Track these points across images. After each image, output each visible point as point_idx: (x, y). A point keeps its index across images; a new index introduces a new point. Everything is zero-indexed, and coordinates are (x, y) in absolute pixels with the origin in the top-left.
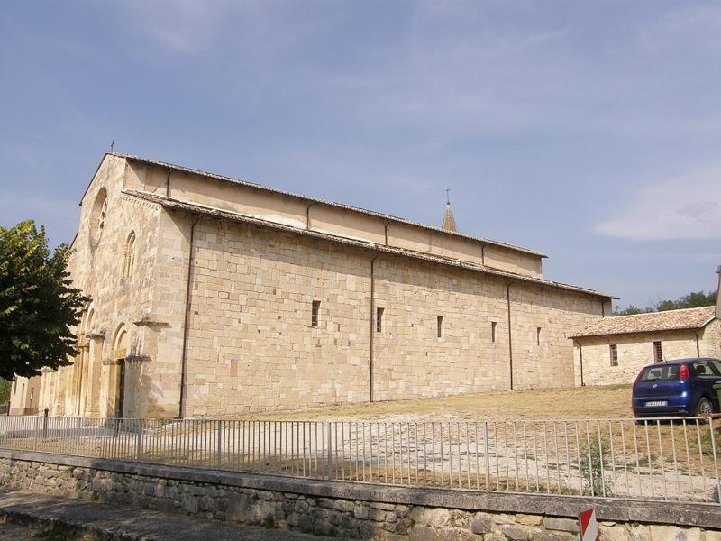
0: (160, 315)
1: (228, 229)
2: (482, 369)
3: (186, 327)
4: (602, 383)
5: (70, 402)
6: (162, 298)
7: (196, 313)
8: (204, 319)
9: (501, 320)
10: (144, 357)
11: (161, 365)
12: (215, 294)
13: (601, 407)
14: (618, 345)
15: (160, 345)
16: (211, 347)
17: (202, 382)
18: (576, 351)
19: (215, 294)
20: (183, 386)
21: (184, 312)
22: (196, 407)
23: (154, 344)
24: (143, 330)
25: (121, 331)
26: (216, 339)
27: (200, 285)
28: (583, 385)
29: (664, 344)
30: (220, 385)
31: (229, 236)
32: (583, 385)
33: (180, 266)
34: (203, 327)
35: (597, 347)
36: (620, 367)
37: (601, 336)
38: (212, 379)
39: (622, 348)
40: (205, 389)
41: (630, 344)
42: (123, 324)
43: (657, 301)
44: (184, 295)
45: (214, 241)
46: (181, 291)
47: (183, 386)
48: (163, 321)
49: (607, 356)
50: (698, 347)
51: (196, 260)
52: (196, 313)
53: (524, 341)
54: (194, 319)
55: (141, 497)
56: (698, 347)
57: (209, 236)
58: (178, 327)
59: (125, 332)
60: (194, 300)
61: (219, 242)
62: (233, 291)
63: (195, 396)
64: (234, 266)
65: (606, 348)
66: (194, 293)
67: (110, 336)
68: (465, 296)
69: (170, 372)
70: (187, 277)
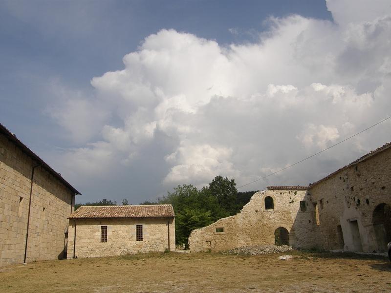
2: (8, 242)
4: (92, 256)
7: (289, 192)
9: (26, 196)
14: (108, 226)
18: (71, 230)
28: (75, 257)
29: (145, 227)
32: (75, 257)
35: (91, 226)
36: (109, 243)
37: (96, 219)
39: (111, 229)
41: (118, 226)
43: (100, 200)
49: (99, 234)
50: (169, 230)
52: (289, 192)
53: (38, 219)
55: (310, 228)
56: (169, 230)
65: (98, 228)
68: (7, 168)
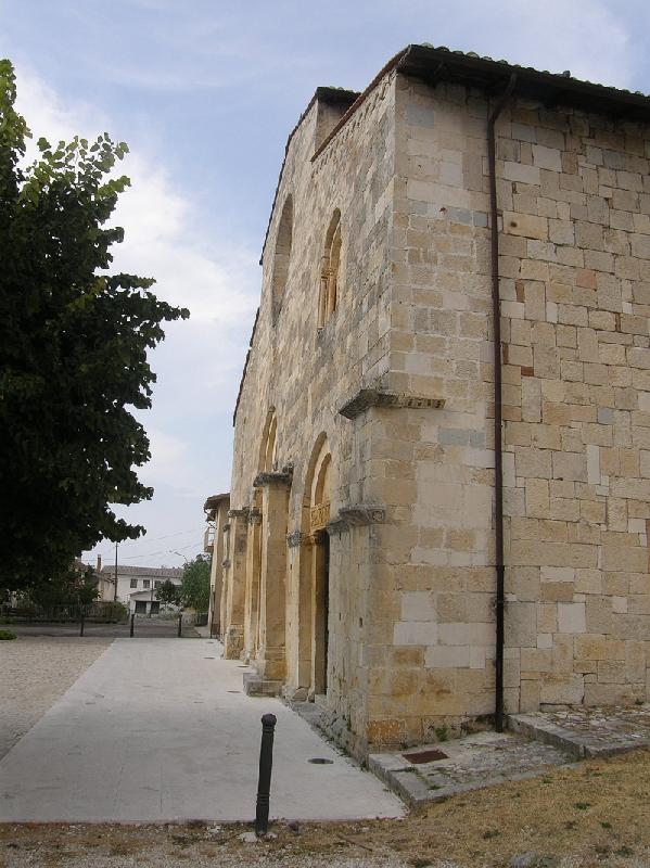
0: (417, 372)
1: (592, 136)
3: (498, 414)
5: (491, 739)
6: (420, 322)
8: (554, 391)
10: (374, 512)
11: (430, 537)
12: (580, 317)
13: (388, 712)
15: (425, 472)
16: (580, 480)
17: (561, 594)
19: (580, 317)
20: (500, 606)
21: (491, 366)
22: (549, 678)
23: (403, 469)
24: (373, 425)
25: (321, 459)
26: (593, 452)
27: (528, 289)
30: (620, 604)
31: (594, 155)
33: (464, 231)
34: (547, 414)
38: (591, 581)
40: (572, 619)
42: (323, 437)
44: (483, 316)
45: (557, 166)
46: (475, 304)
47: (500, 606)
48: (431, 393)
51: (508, 216)
52: (528, 372)
54: (523, 394)
57: (538, 151)
58: (473, 417)
59: (328, 458)
60: (517, 333)
61: (570, 169)
62: (627, 308)
63: (544, 642)
64: (622, 239)
66: (512, 309)
67: (300, 477)
69: (460, 559)
70: (488, 264)
